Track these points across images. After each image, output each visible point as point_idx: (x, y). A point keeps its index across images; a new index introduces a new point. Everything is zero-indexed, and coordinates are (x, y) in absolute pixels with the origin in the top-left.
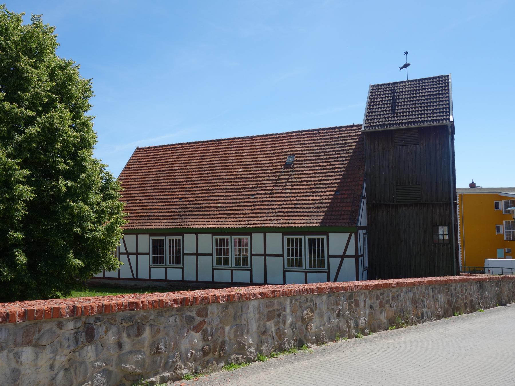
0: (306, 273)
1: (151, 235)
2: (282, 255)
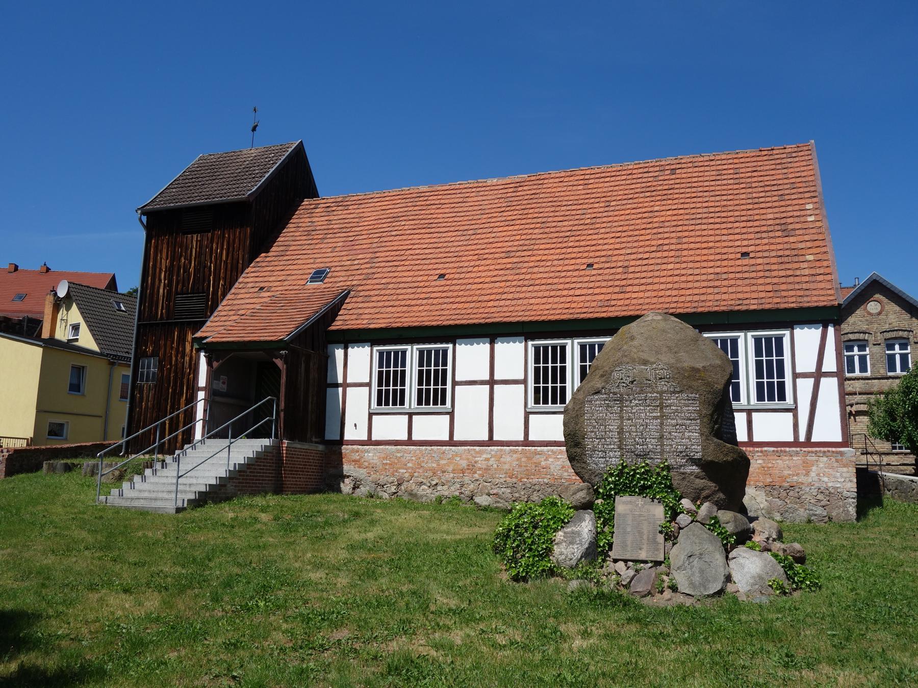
0: (410, 415)
1: (373, 343)
2: (369, 385)
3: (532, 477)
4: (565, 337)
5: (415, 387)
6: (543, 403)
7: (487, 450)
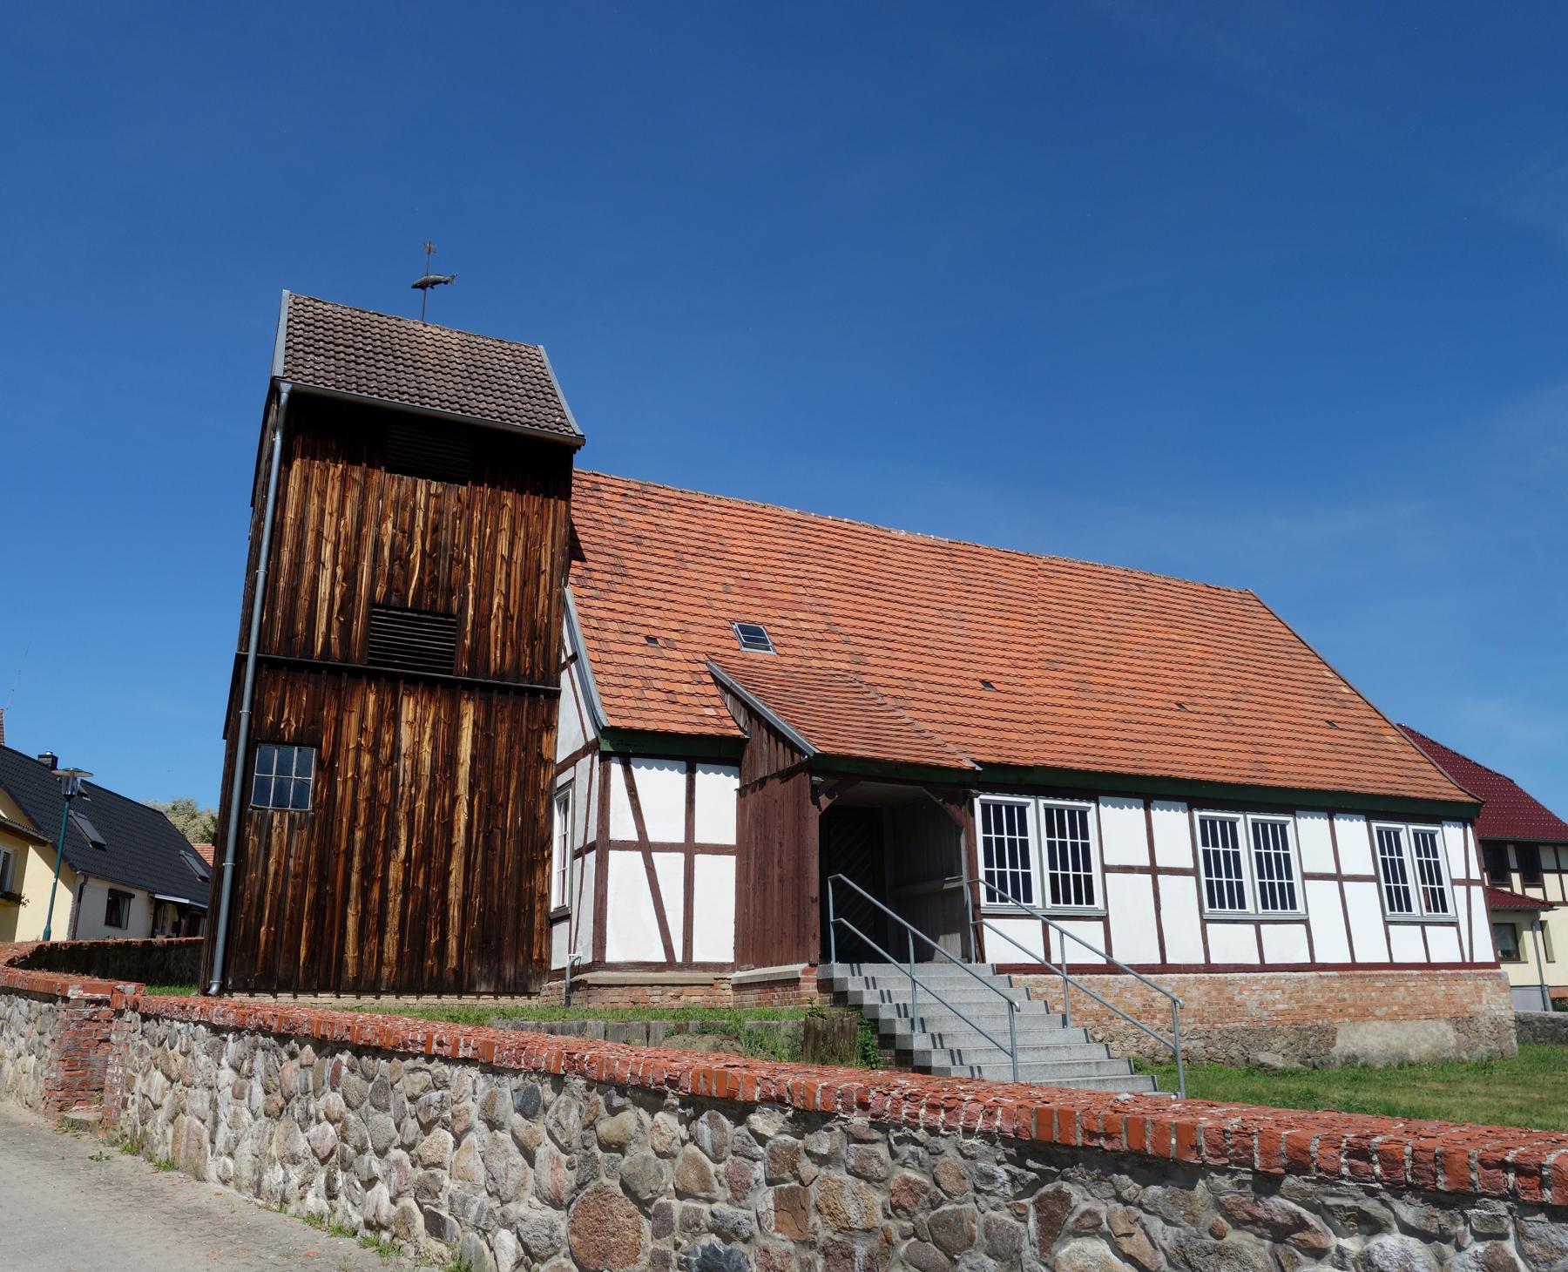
1: (1370, 816)
3: (1227, 1020)
4: (1237, 810)
5: (1034, 870)
6: (1240, 908)
7: (1164, 979)
